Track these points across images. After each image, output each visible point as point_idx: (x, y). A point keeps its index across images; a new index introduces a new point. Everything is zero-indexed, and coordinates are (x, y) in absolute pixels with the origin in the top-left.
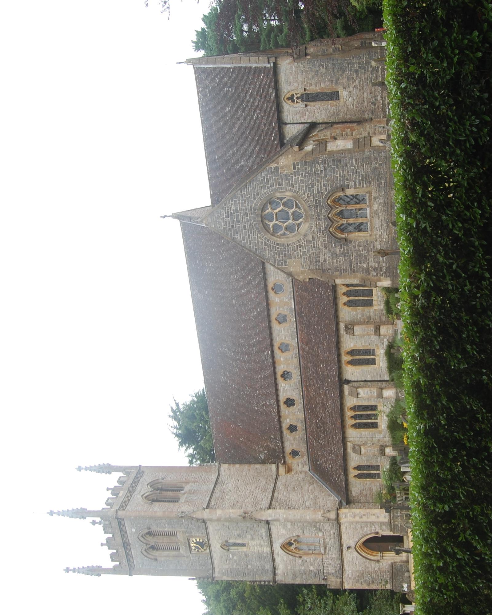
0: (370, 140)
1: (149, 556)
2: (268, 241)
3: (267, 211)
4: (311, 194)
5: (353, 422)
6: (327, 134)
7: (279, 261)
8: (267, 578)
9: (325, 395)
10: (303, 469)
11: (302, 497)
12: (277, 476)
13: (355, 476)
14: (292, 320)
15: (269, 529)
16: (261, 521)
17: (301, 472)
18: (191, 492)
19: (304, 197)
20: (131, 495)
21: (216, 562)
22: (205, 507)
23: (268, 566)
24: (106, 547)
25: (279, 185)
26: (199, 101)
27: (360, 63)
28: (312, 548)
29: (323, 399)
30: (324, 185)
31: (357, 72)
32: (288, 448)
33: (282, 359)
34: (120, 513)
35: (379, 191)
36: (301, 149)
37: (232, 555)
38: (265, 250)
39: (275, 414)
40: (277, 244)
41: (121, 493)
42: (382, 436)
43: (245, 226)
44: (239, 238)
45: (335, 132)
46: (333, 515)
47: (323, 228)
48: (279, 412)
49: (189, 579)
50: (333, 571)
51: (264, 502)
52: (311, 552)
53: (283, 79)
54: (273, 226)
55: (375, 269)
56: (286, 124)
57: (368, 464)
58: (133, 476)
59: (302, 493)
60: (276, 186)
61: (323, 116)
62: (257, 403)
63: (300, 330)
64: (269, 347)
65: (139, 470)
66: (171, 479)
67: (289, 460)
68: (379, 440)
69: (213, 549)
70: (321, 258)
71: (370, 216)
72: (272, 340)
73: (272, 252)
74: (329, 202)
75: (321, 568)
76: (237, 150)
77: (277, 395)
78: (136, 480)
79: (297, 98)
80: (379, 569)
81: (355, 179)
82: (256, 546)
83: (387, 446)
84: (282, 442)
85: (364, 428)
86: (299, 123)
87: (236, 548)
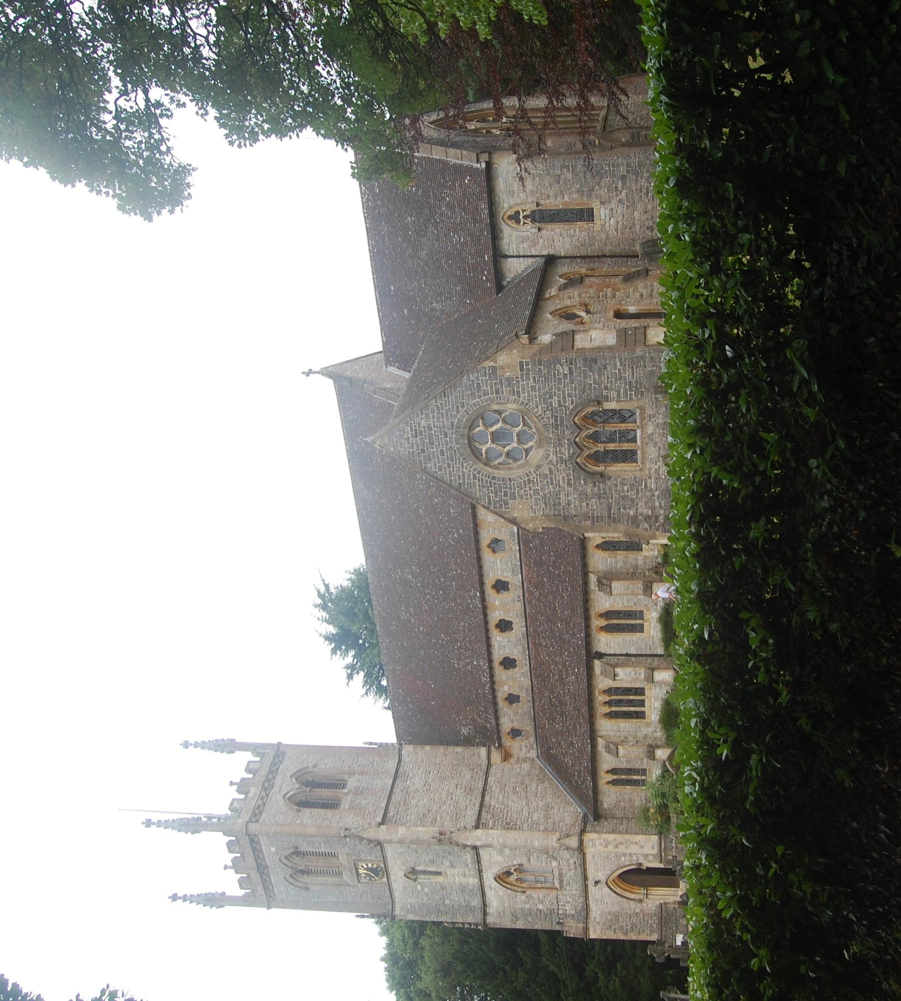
0: (645, 334)
1: (296, 883)
2: (479, 472)
3: (477, 429)
4: (547, 408)
5: (607, 709)
6: (571, 299)
7: (495, 503)
8: (473, 919)
9: (564, 665)
10: (528, 755)
11: (527, 804)
12: (489, 765)
13: (608, 783)
14: (514, 548)
15: (478, 855)
16: (465, 846)
17: (525, 760)
18: (358, 792)
19: (537, 412)
20: (267, 795)
21: (397, 894)
22: (379, 819)
23: (476, 902)
24: (233, 871)
25: (497, 393)
26: (362, 198)
27: (628, 165)
28: (542, 879)
29: (561, 671)
30: (569, 395)
31: (623, 178)
32: (506, 724)
33: (497, 603)
34: (253, 827)
35: (656, 406)
36: (532, 340)
37: (422, 886)
38: (474, 485)
39: (485, 679)
40: (494, 478)
41: (253, 791)
42: (650, 730)
43: (442, 451)
44: (433, 467)
45: (587, 292)
46: (573, 842)
47: (566, 456)
48: (492, 676)
49: (358, 916)
50: (573, 912)
51: (469, 813)
52: (539, 885)
53: (502, 188)
54: (486, 452)
55: (647, 518)
56: (507, 257)
57: (629, 767)
58: (269, 759)
59: (526, 797)
60: (492, 394)
61: (567, 246)
62: (459, 659)
63: (527, 565)
64: (477, 586)
65: (278, 749)
66: (326, 768)
67: (507, 742)
68: (646, 735)
69: (392, 878)
70: (563, 500)
71: (642, 442)
72: (481, 576)
73: (485, 489)
74: (576, 420)
75: (555, 907)
76: (426, 284)
77: (490, 653)
78: (274, 769)
79: (525, 217)
80: (641, 910)
81: (619, 387)
82: (458, 875)
83: (658, 747)
84: (497, 718)
85: (624, 717)
86: (528, 256)
87: (427, 877)
